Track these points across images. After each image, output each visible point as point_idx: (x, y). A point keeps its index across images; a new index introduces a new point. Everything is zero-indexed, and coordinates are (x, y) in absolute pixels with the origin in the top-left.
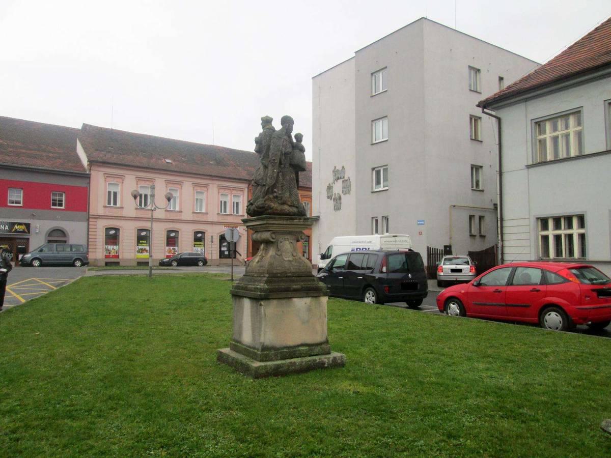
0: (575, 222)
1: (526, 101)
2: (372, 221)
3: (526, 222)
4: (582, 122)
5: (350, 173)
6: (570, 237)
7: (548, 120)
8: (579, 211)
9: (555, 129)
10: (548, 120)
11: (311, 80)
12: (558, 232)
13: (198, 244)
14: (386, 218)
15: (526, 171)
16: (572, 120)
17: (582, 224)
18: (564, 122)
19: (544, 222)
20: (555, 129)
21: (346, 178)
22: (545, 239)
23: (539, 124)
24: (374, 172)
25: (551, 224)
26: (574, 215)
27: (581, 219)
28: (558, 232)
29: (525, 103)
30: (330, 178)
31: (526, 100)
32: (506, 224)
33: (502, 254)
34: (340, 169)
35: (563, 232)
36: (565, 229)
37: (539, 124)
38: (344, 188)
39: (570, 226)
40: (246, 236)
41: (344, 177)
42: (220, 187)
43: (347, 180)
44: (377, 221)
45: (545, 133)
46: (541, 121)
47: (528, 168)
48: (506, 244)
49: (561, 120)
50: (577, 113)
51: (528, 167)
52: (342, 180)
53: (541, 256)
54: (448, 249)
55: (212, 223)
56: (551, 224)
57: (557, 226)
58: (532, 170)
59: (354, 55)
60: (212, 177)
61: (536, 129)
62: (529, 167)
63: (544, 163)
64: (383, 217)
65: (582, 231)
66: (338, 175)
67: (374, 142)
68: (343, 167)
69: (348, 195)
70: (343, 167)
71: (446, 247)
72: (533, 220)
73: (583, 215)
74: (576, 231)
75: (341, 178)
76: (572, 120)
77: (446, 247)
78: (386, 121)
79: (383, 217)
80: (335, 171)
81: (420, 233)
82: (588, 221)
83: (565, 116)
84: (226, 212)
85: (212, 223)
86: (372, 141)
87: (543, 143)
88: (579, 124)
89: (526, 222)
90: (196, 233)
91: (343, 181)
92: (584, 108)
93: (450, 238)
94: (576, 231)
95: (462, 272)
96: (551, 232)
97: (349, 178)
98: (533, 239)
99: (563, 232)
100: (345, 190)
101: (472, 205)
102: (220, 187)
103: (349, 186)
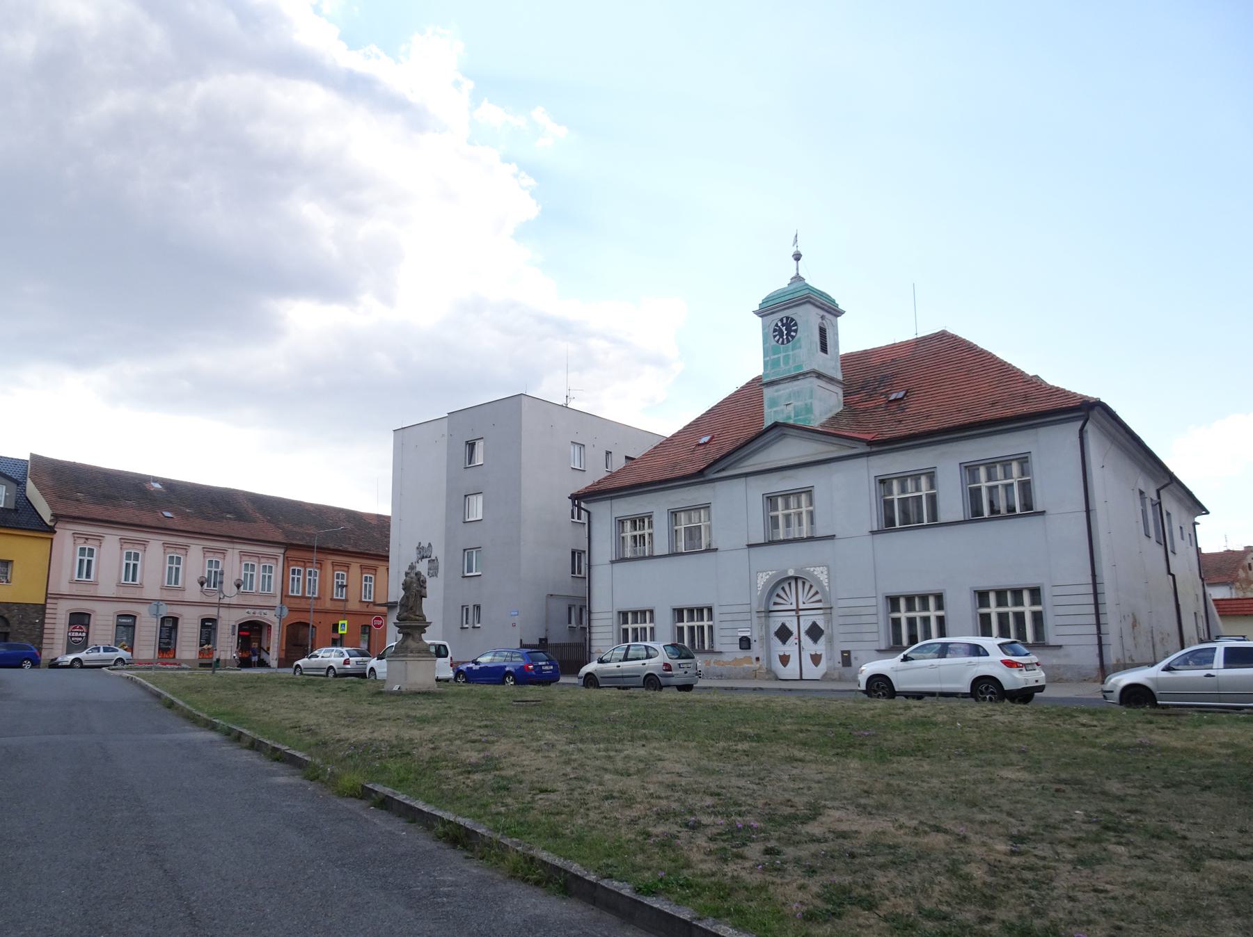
0: (1026, 597)
1: (868, 456)
2: (463, 610)
3: (610, 615)
4: (936, 486)
5: (438, 552)
6: (926, 620)
7: (781, 496)
8: (1033, 582)
9: (787, 507)
10: (781, 496)
11: (392, 433)
12: (911, 614)
13: (312, 635)
14: (478, 607)
15: (870, 538)
16: (804, 497)
17: (940, 606)
18: (796, 498)
19: (893, 602)
20: (787, 507)
21: (433, 558)
22: (896, 623)
23: (771, 500)
24: (466, 553)
25: (992, 598)
26: (991, 590)
27: (939, 598)
28: (911, 614)
29: (866, 458)
30: (414, 556)
31: (612, 498)
32: (594, 616)
33: (590, 646)
34: (426, 546)
35: (918, 614)
36: (697, 621)
37: (771, 500)
38: (429, 569)
39: (1018, 601)
40: (278, 625)
41: (430, 557)
42: (243, 554)
43: (434, 560)
44: (467, 609)
45: (776, 509)
46: (678, 512)
47: (873, 534)
48: (594, 636)
49: (912, 480)
50: (707, 507)
51: (873, 533)
52: (428, 559)
53: (892, 644)
54: (543, 642)
55: (229, 606)
56: (992, 598)
57: (1001, 602)
58: (614, 565)
59: (447, 415)
60: (232, 539)
61: (767, 504)
62: (612, 562)
63: (624, 560)
64: (474, 606)
65: (940, 613)
66: (423, 553)
67: (467, 520)
68: (430, 545)
69: (435, 577)
70: (430, 545)
71: (541, 640)
72: (615, 613)
73: (942, 593)
74: (933, 614)
75: (426, 557)
76: (804, 497)
77: (541, 640)
78: (480, 498)
79: (474, 606)
80: (420, 548)
81: (514, 625)
82: (948, 600)
83: (797, 493)
84: (270, 591)
85: (229, 606)
86: (464, 519)
87: (775, 520)
88: (811, 504)
89: (610, 615)
90: (204, 621)
91: (429, 561)
92: (938, 469)
93: (547, 630)
94: (1027, 609)
95: (200, 664)
96: (993, 610)
97: (436, 557)
98: (615, 632)
99: (1011, 609)
100: (431, 572)
101: (571, 594)
102: (243, 554)
103: (437, 568)
